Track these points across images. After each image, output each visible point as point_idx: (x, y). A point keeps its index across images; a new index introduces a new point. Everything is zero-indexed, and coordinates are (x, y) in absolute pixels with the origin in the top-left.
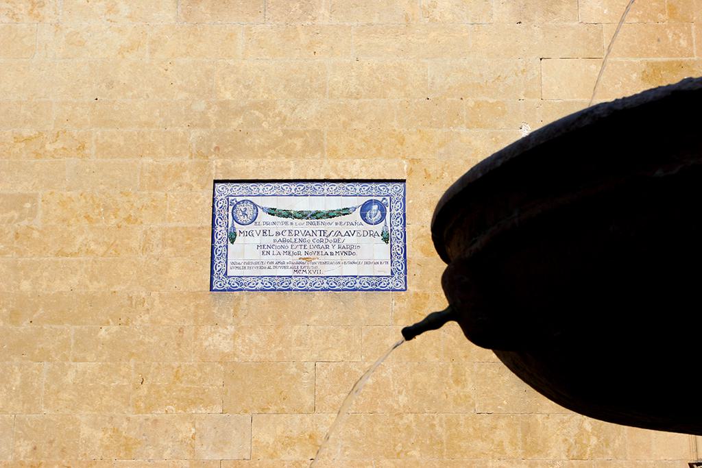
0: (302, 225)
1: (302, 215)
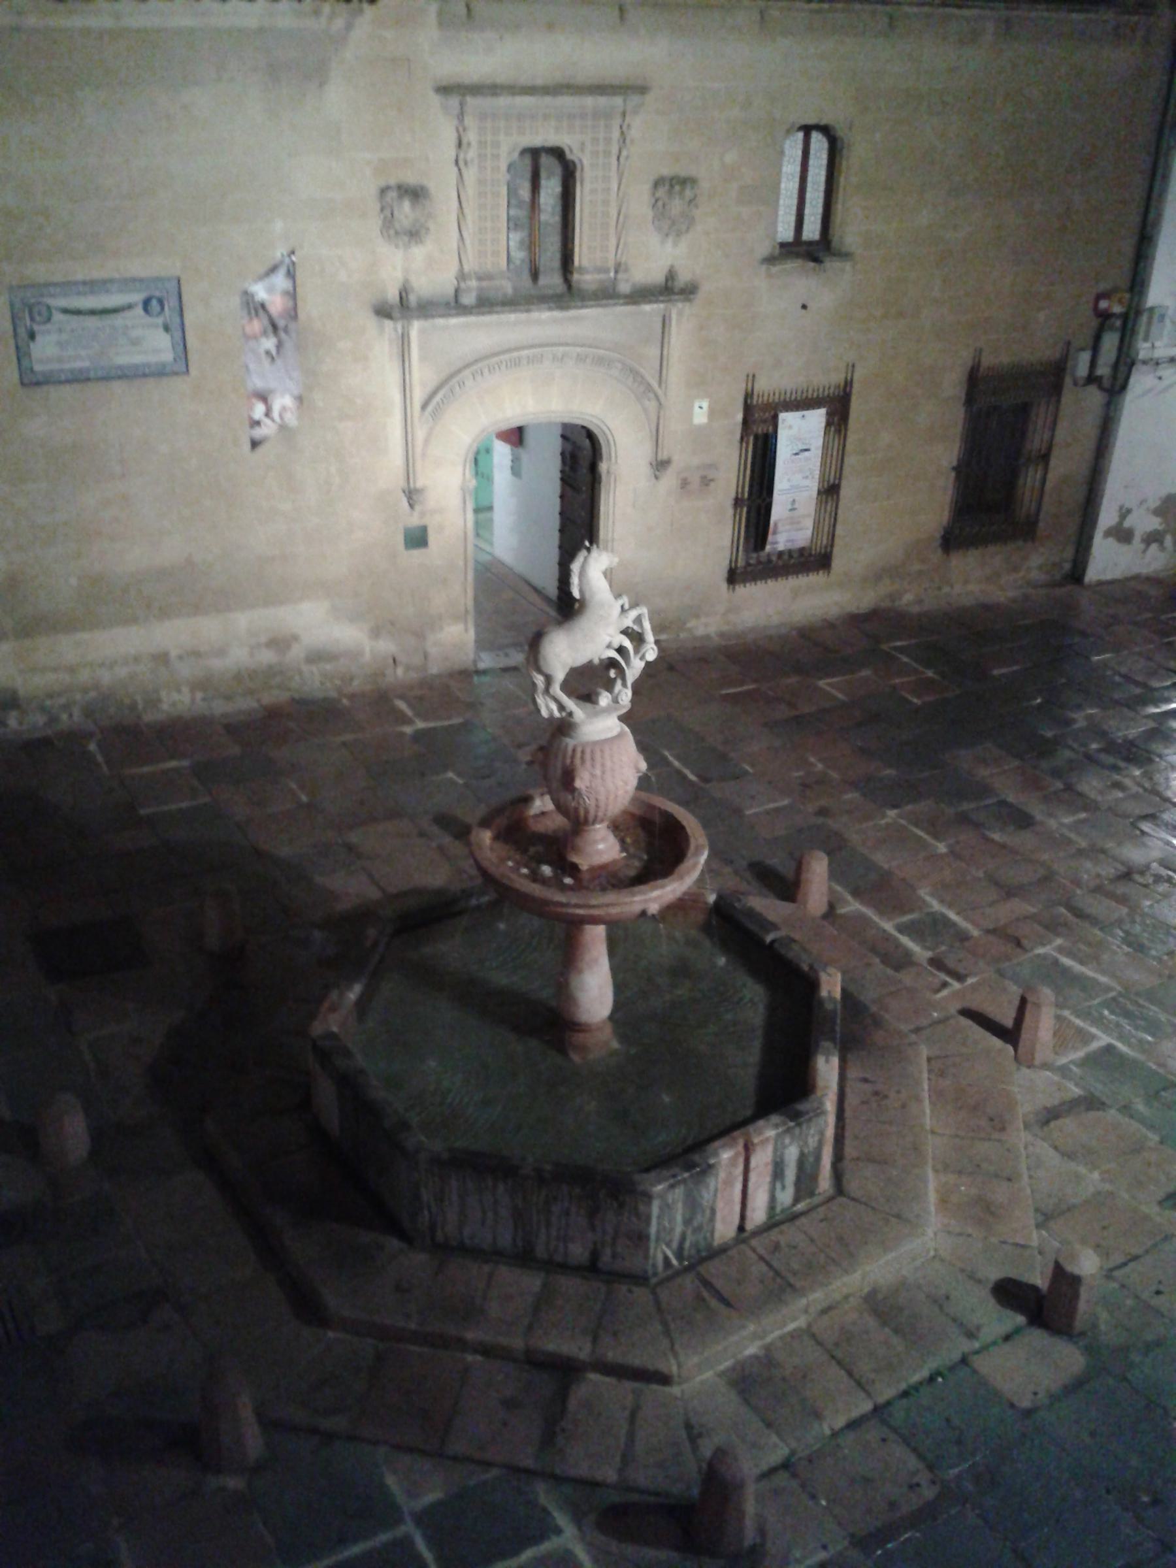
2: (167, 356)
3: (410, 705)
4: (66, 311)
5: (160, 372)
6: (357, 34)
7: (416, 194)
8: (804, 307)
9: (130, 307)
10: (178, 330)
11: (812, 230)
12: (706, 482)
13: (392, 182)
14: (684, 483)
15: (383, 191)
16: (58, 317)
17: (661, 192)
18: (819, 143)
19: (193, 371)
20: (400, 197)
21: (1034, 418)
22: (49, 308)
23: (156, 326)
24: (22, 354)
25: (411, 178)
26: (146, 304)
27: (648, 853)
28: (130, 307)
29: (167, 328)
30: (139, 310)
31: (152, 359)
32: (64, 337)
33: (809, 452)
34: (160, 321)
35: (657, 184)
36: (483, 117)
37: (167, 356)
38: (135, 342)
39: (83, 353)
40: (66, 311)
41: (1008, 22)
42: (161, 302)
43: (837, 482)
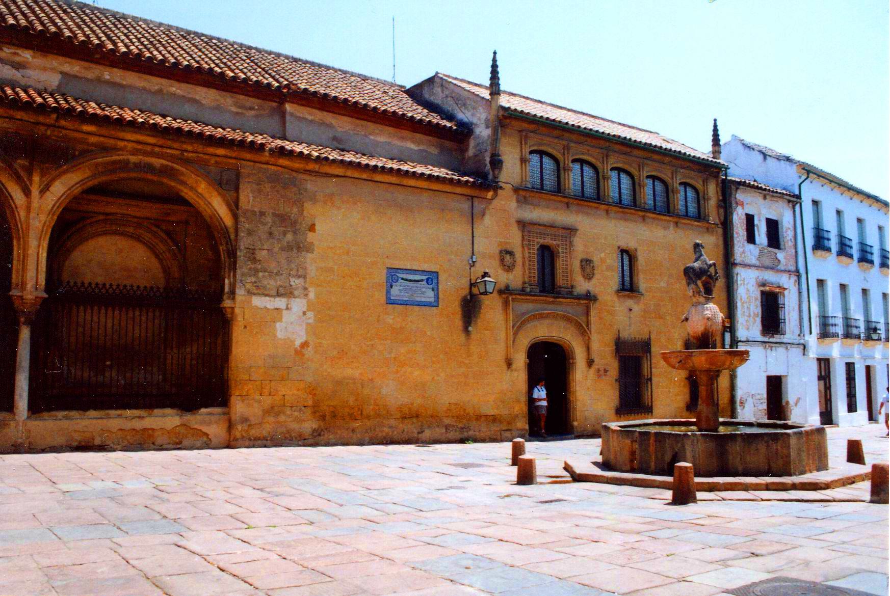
0: (411, 284)
1: (411, 281)
2: (432, 300)
3: (378, 142)
4: (402, 279)
5: (429, 305)
6: (495, 202)
7: (511, 253)
8: (631, 310)
9: (422, 280)
10: (436, 290)
11: (627, 283)
12: (606, 371)
13: (504, 249)
14: (599, 370)
15: (501, 252)
16: (400, 280)
17: (584, 263)
18: (626, 258)
19: (440, 306)
20: (506, 253)
21: (718, 189)
22: (398, 277)
23: (429, 288)
24: (388, 292)
25: (509, 248)
26: (427, 279)
27: (10, 297)
28: (422, 280)
29: (433, 290)
30: (424, 282)
31: (428, 300)
32: (401, 288)
33: (570, 463)
34: (431, 286)
35: (581, 261)
36: (529, 232)
37: (432, 300)
38: (423, 293)
39: (407, 294)
40: (402, 279)
41: (676, 223)
42: (432, 280)
43: (649, 377)
